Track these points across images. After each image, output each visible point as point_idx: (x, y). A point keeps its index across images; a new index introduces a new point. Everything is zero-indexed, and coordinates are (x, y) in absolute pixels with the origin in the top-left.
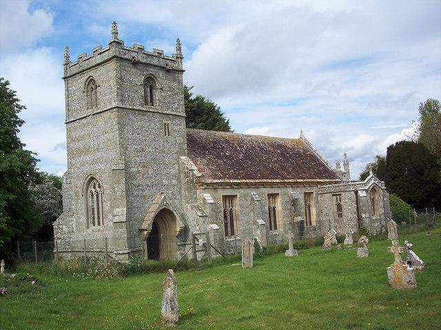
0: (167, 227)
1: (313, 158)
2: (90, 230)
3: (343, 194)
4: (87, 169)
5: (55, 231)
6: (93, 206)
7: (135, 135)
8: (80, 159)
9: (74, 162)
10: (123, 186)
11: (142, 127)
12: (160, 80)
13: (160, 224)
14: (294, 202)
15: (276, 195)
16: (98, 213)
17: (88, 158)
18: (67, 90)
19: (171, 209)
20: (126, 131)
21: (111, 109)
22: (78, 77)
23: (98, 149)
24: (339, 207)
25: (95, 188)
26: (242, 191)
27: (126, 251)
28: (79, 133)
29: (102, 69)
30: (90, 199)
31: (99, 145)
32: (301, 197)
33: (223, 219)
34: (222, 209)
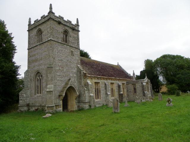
0: (72, 97)
2: (36, 96)
4: (36, 68)
5: (20, 96)
6: (38, 85)
7: (59, 53)
8: (33, 64)
9: (30, 65)
11: (62, 51)
12: (70, 33)
13: (68, 93)
14: (119, 86)
15: (113, 83)
16: (40, 88)
17: (37, 64)
18: (29, 35)
19: (74, 87)
20: (54, 51)
21: (48, 41)
22: (34, 29)
23: (41, 59)
25: (39, 77)
26: (102, 80)
28: (33, 53)
29: (45, 25)
30: (37, 82)
31: (42, 58)
32: (121, 84)
33: (95, 92)
34: (95, 87)
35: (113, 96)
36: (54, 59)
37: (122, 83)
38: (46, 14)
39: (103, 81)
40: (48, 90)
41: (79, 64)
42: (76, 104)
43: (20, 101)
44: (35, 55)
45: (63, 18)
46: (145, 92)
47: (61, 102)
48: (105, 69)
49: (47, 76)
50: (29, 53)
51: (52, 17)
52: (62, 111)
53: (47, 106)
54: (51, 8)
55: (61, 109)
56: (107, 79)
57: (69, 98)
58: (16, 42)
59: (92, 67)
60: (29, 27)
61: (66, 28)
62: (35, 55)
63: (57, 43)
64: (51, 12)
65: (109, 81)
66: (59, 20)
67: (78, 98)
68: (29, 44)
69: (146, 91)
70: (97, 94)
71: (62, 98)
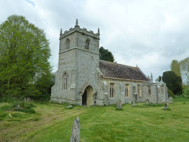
1: (97, 95)
2: (63, 91)
3: (151, 86)
4: (64, 69)
10: (75, 76)
13: (88, 91)
14: (134, 88)
17: (64, 66)
18: (60, 43)
23: (68, 63)
24: (150, 91)
27: (74, 100)
30: (64, 80)
32: (137, 86)
35: (127, 95)
36: (78, 63)
37: (138, 85)
38: (73, 27)
39: (118, 82)
40: (71, 87)
41: (98, 67)
42: (94, 100)
43: (52, 94)
44: (63, 59)
45: (86, 29)
46: (159, 94)
47: (81, 98)
48: (122, 71)
49: (71, 76)
50: (59, 57)
51: (77, 30)
52: (81, 105)
53: (70, 99)
54: (77, 23)
55: (80, 102)
56: (122, 81)
57: (88, 95)
58: (51, 46)
59: (109, 70)
60: (60, 36)
61: (89, 37)
62: (63, 59)
63: (80, 51)
64: (77, 26)
65: (124, 82)
66: (83, 31)
67: (95, 95)
68: (60, 50)
69: (159, 94)
70: (111, 93)
71: (82, 94)
